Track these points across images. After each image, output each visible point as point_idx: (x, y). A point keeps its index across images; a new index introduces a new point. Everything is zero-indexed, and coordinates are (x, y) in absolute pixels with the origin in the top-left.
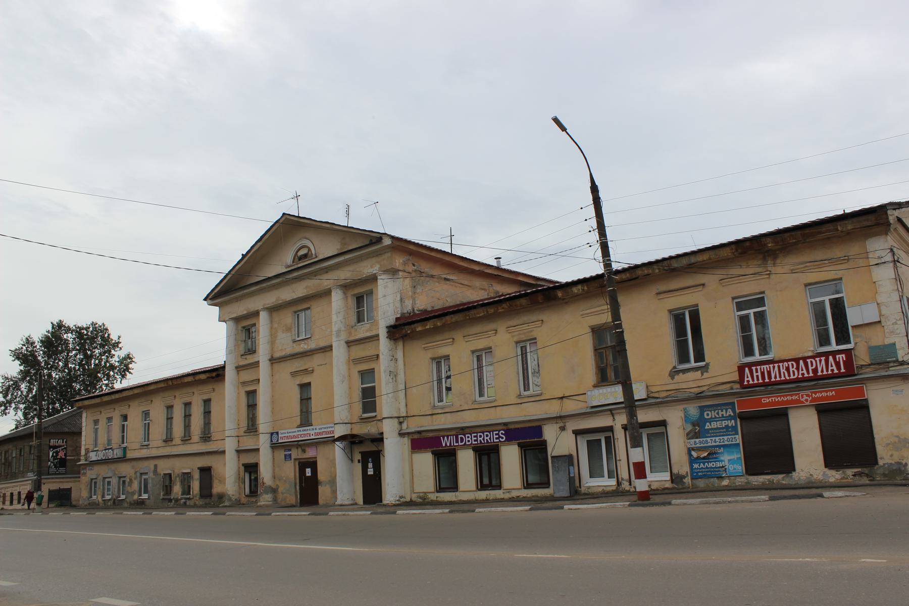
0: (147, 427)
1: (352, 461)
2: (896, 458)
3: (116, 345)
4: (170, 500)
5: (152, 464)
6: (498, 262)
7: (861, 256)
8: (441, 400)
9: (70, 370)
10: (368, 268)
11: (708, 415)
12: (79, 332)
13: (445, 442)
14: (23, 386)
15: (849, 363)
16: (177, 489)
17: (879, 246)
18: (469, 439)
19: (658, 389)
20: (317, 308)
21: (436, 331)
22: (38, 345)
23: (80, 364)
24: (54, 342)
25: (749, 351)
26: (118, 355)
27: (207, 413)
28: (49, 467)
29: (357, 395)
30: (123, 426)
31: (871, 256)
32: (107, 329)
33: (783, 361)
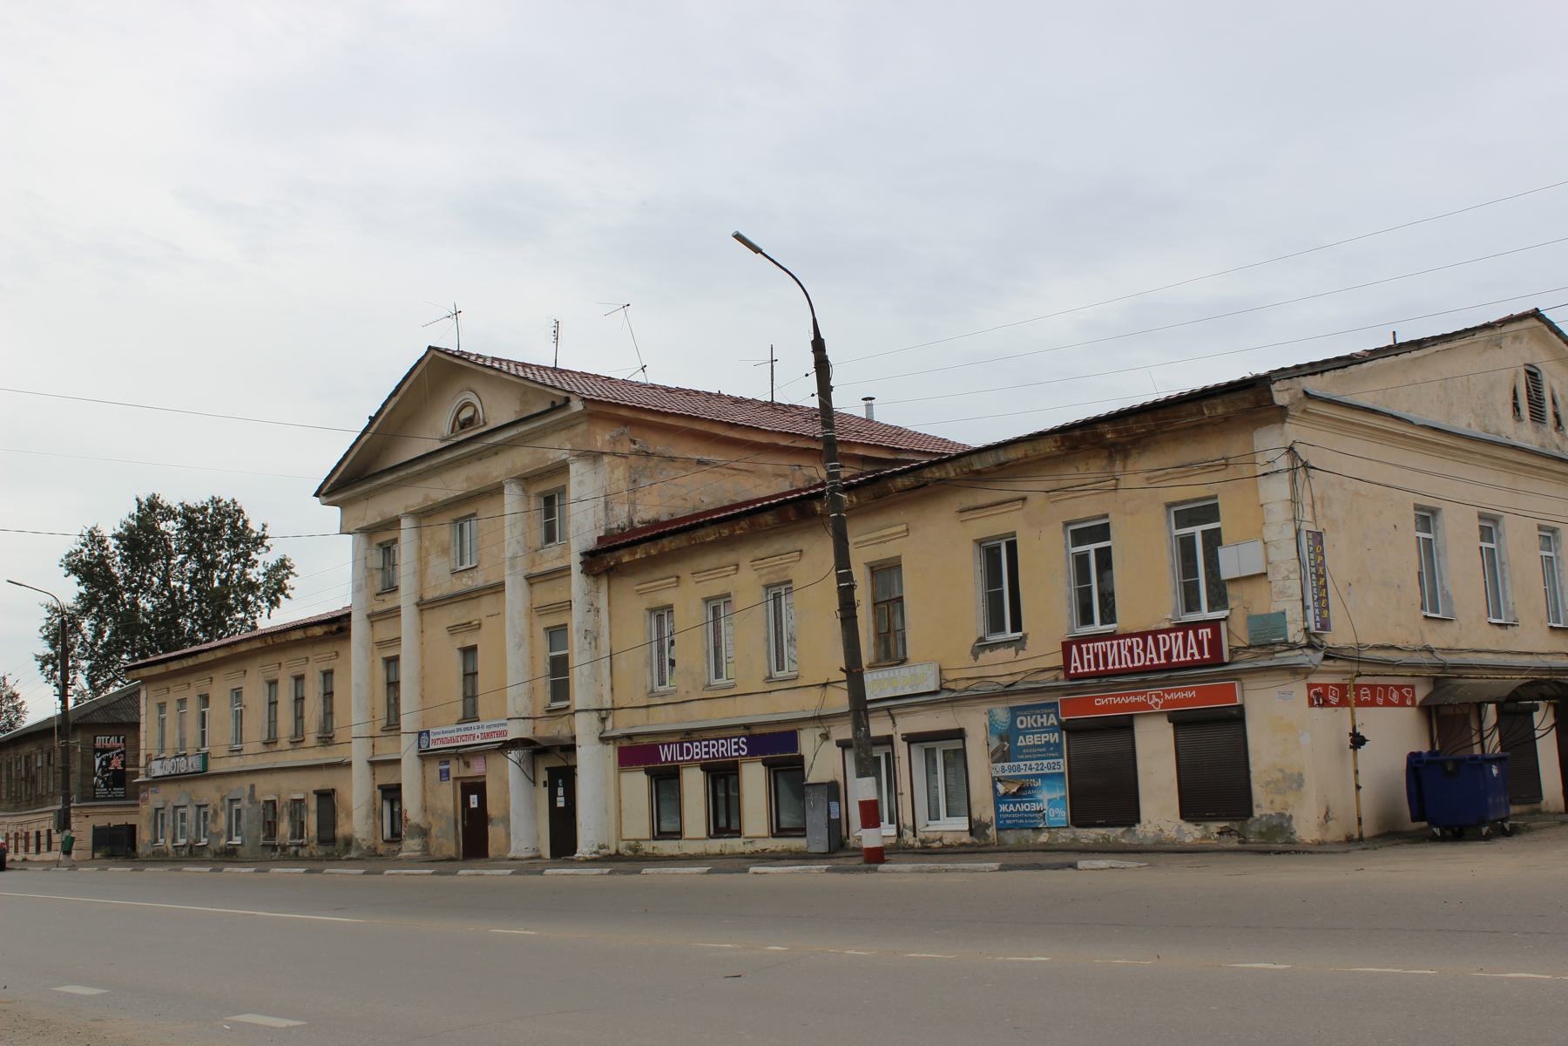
0: (239, 716)
1: (534, 782)
2: (1278, 808)
3: (259, 541)
4: (274, 848)
5: (246, 782)
6: (869, 408)
7: (1243, 460)
8: (662, 683)
9: (173, 593)
10: (555, 449)
11: (1024, 722)
12: (189, 517)
13: (666, 754)
14: (86, 624)
15: (1215, 643)
16: (284, 827)
17: (1269, 442)
18: (698, 750)
19: (955, 675)
20: (485, 509)
21: (652, 562)
22: (112, 543)
23: (193, 581)
24: (142, 537)
25: (1086, 618)
26: (264, 559)
27: (328, 695)
28: (95, 786)
29: (543, 667)
30: (204, 714)
31: (1260, 459)
32: (240, 511)
33: (1124, 636)
